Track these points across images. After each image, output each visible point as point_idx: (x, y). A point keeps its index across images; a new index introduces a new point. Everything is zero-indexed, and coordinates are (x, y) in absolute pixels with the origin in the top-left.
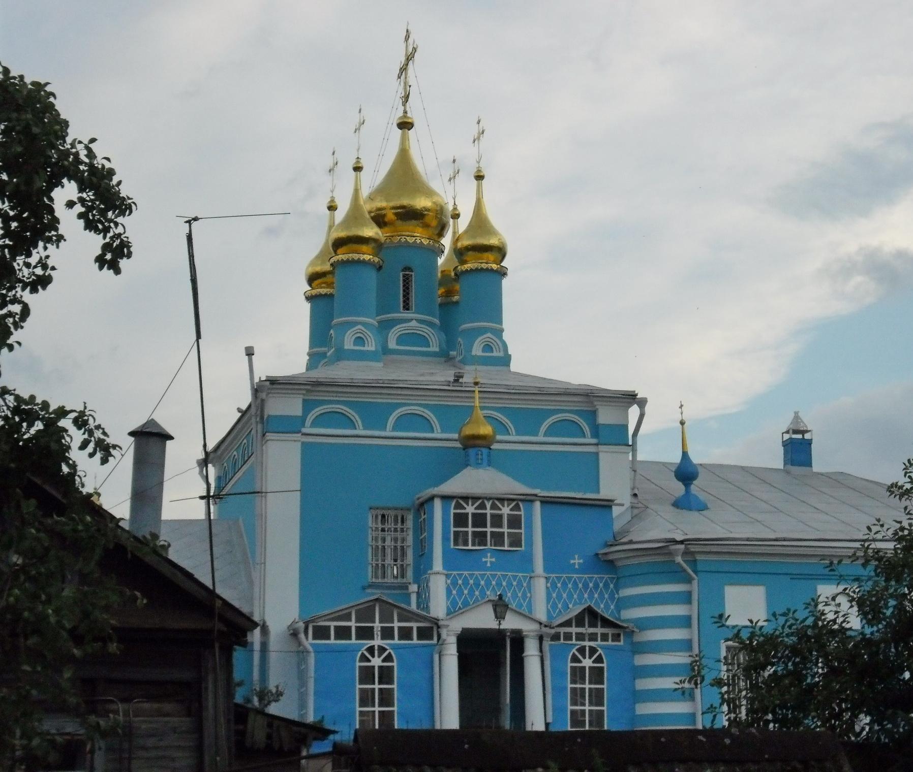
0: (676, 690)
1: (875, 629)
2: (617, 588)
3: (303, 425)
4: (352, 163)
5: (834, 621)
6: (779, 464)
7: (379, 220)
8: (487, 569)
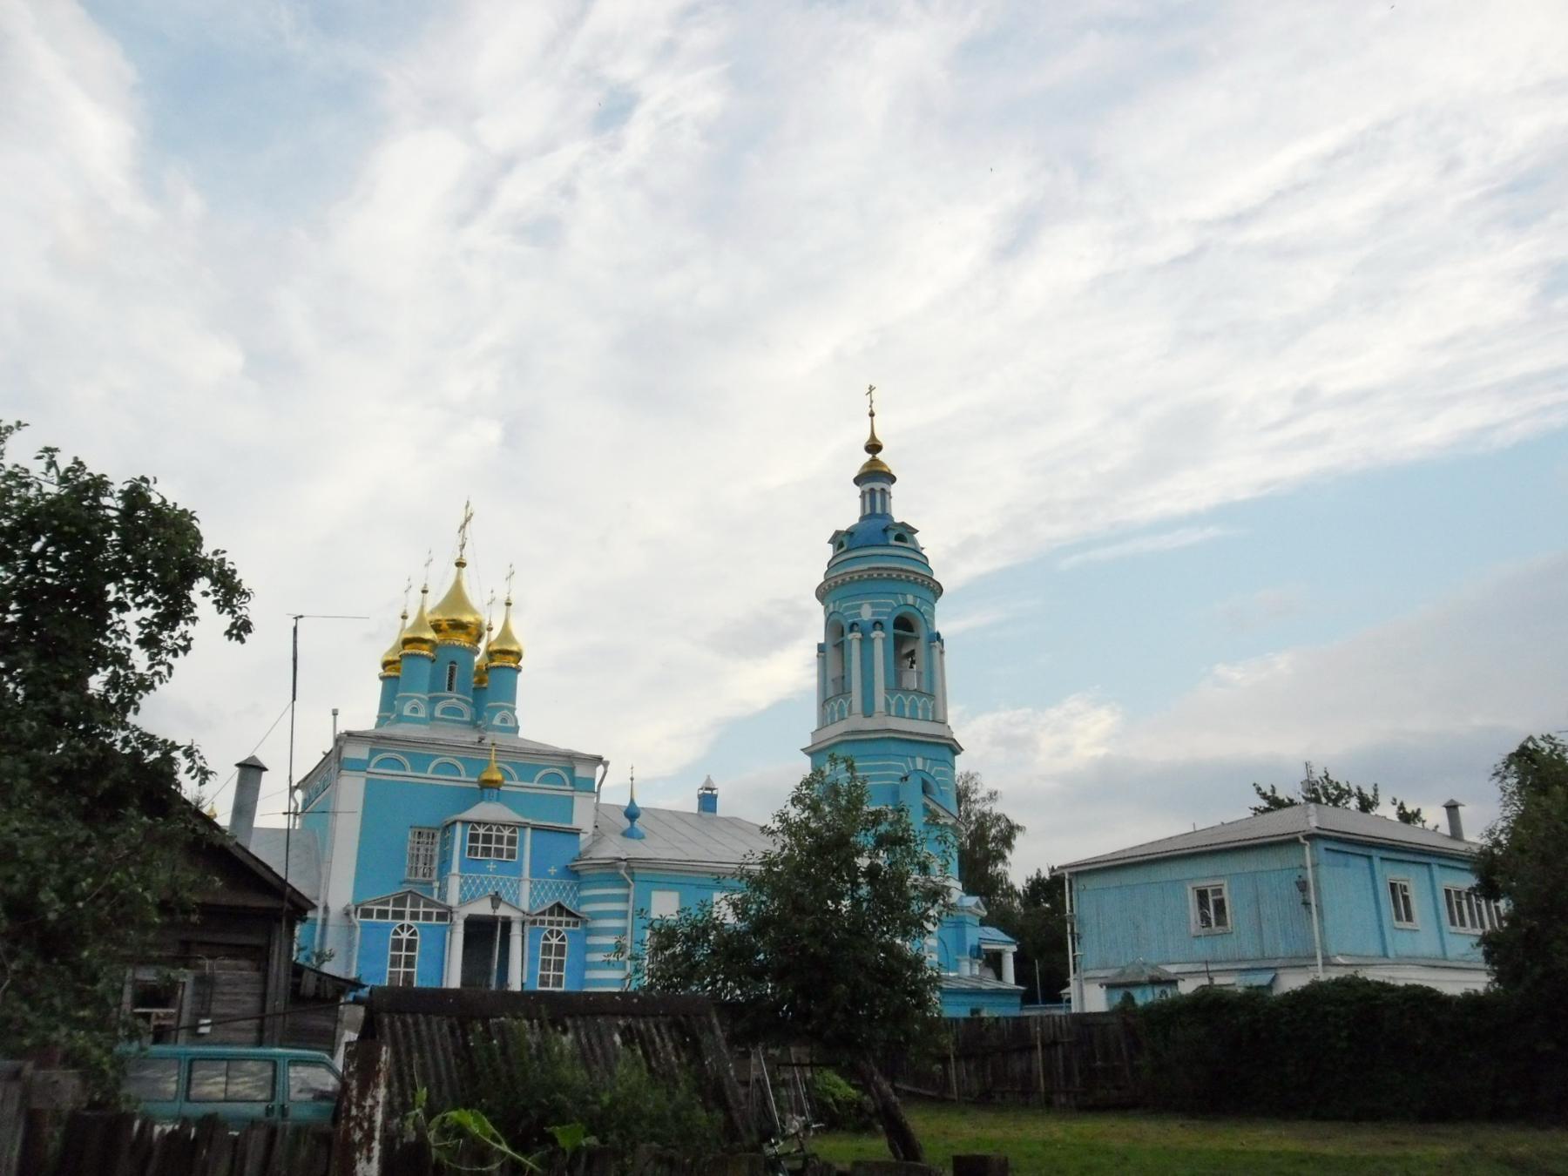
0: (604, 961)
1: (743, 924)
2: (579, 890)
3: (368, 766)
4: (421, 587)
5: (717, 918)
6: (695, 810)
7: (436, 627)
8: (489, 873)
